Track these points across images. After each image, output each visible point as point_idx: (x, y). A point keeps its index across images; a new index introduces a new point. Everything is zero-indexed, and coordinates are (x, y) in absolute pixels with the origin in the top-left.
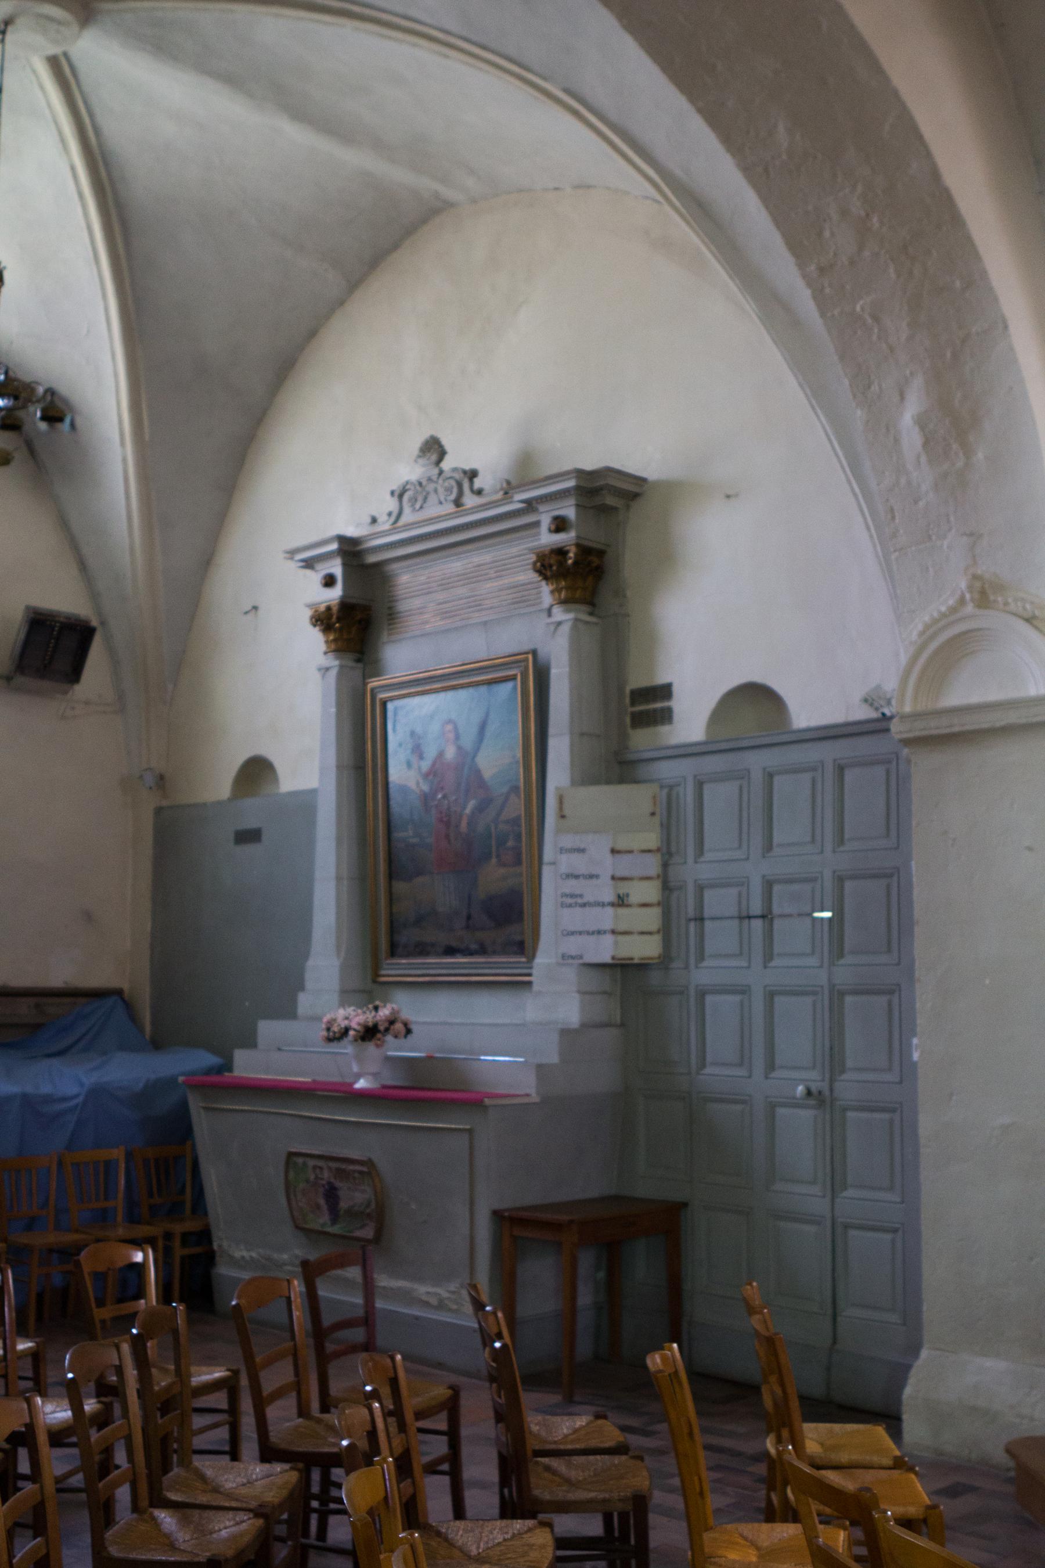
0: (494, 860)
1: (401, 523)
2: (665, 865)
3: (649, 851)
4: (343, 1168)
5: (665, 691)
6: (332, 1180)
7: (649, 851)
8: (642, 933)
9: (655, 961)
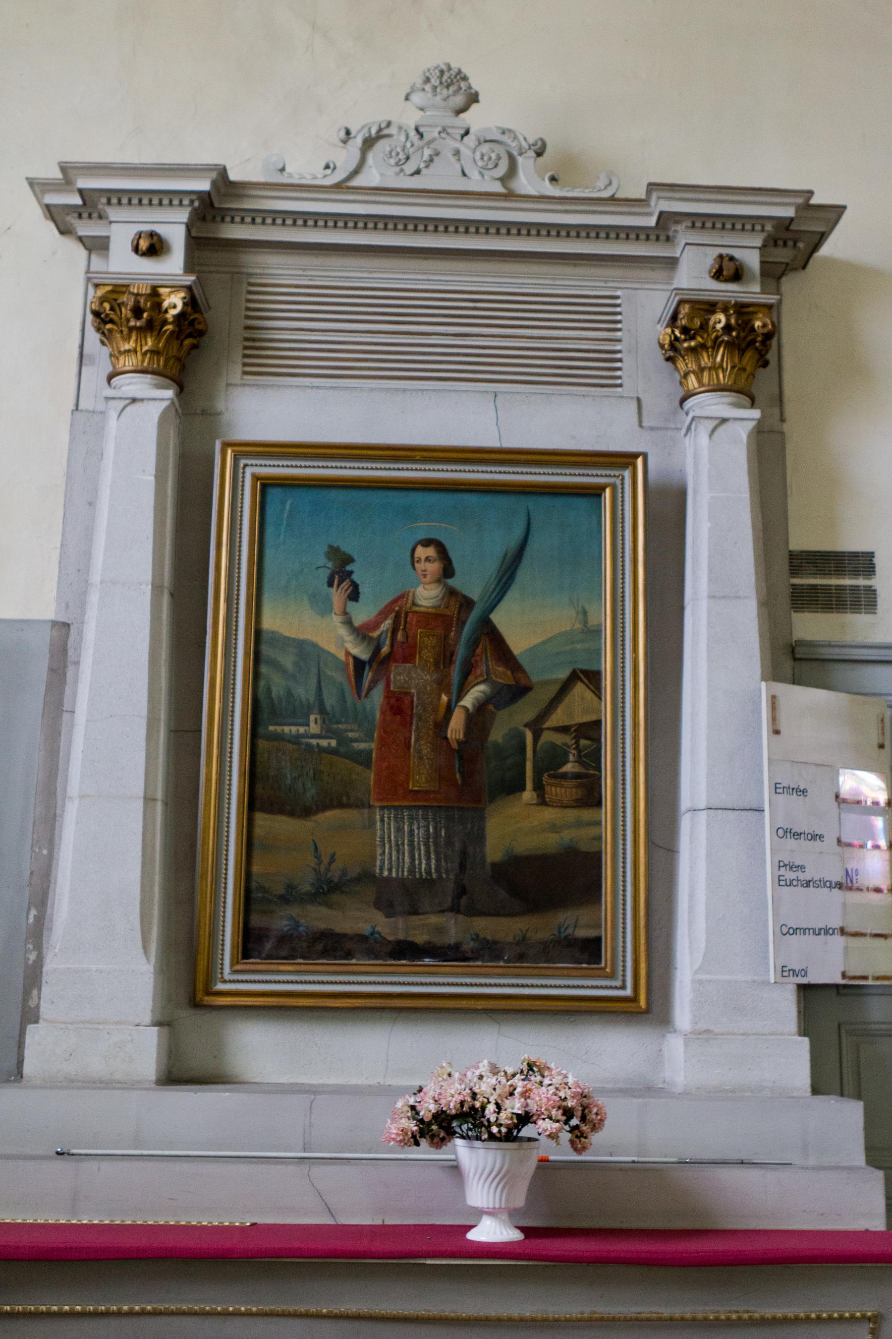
0: (528, 795)
1: (357, 182)
5: (864, 563)
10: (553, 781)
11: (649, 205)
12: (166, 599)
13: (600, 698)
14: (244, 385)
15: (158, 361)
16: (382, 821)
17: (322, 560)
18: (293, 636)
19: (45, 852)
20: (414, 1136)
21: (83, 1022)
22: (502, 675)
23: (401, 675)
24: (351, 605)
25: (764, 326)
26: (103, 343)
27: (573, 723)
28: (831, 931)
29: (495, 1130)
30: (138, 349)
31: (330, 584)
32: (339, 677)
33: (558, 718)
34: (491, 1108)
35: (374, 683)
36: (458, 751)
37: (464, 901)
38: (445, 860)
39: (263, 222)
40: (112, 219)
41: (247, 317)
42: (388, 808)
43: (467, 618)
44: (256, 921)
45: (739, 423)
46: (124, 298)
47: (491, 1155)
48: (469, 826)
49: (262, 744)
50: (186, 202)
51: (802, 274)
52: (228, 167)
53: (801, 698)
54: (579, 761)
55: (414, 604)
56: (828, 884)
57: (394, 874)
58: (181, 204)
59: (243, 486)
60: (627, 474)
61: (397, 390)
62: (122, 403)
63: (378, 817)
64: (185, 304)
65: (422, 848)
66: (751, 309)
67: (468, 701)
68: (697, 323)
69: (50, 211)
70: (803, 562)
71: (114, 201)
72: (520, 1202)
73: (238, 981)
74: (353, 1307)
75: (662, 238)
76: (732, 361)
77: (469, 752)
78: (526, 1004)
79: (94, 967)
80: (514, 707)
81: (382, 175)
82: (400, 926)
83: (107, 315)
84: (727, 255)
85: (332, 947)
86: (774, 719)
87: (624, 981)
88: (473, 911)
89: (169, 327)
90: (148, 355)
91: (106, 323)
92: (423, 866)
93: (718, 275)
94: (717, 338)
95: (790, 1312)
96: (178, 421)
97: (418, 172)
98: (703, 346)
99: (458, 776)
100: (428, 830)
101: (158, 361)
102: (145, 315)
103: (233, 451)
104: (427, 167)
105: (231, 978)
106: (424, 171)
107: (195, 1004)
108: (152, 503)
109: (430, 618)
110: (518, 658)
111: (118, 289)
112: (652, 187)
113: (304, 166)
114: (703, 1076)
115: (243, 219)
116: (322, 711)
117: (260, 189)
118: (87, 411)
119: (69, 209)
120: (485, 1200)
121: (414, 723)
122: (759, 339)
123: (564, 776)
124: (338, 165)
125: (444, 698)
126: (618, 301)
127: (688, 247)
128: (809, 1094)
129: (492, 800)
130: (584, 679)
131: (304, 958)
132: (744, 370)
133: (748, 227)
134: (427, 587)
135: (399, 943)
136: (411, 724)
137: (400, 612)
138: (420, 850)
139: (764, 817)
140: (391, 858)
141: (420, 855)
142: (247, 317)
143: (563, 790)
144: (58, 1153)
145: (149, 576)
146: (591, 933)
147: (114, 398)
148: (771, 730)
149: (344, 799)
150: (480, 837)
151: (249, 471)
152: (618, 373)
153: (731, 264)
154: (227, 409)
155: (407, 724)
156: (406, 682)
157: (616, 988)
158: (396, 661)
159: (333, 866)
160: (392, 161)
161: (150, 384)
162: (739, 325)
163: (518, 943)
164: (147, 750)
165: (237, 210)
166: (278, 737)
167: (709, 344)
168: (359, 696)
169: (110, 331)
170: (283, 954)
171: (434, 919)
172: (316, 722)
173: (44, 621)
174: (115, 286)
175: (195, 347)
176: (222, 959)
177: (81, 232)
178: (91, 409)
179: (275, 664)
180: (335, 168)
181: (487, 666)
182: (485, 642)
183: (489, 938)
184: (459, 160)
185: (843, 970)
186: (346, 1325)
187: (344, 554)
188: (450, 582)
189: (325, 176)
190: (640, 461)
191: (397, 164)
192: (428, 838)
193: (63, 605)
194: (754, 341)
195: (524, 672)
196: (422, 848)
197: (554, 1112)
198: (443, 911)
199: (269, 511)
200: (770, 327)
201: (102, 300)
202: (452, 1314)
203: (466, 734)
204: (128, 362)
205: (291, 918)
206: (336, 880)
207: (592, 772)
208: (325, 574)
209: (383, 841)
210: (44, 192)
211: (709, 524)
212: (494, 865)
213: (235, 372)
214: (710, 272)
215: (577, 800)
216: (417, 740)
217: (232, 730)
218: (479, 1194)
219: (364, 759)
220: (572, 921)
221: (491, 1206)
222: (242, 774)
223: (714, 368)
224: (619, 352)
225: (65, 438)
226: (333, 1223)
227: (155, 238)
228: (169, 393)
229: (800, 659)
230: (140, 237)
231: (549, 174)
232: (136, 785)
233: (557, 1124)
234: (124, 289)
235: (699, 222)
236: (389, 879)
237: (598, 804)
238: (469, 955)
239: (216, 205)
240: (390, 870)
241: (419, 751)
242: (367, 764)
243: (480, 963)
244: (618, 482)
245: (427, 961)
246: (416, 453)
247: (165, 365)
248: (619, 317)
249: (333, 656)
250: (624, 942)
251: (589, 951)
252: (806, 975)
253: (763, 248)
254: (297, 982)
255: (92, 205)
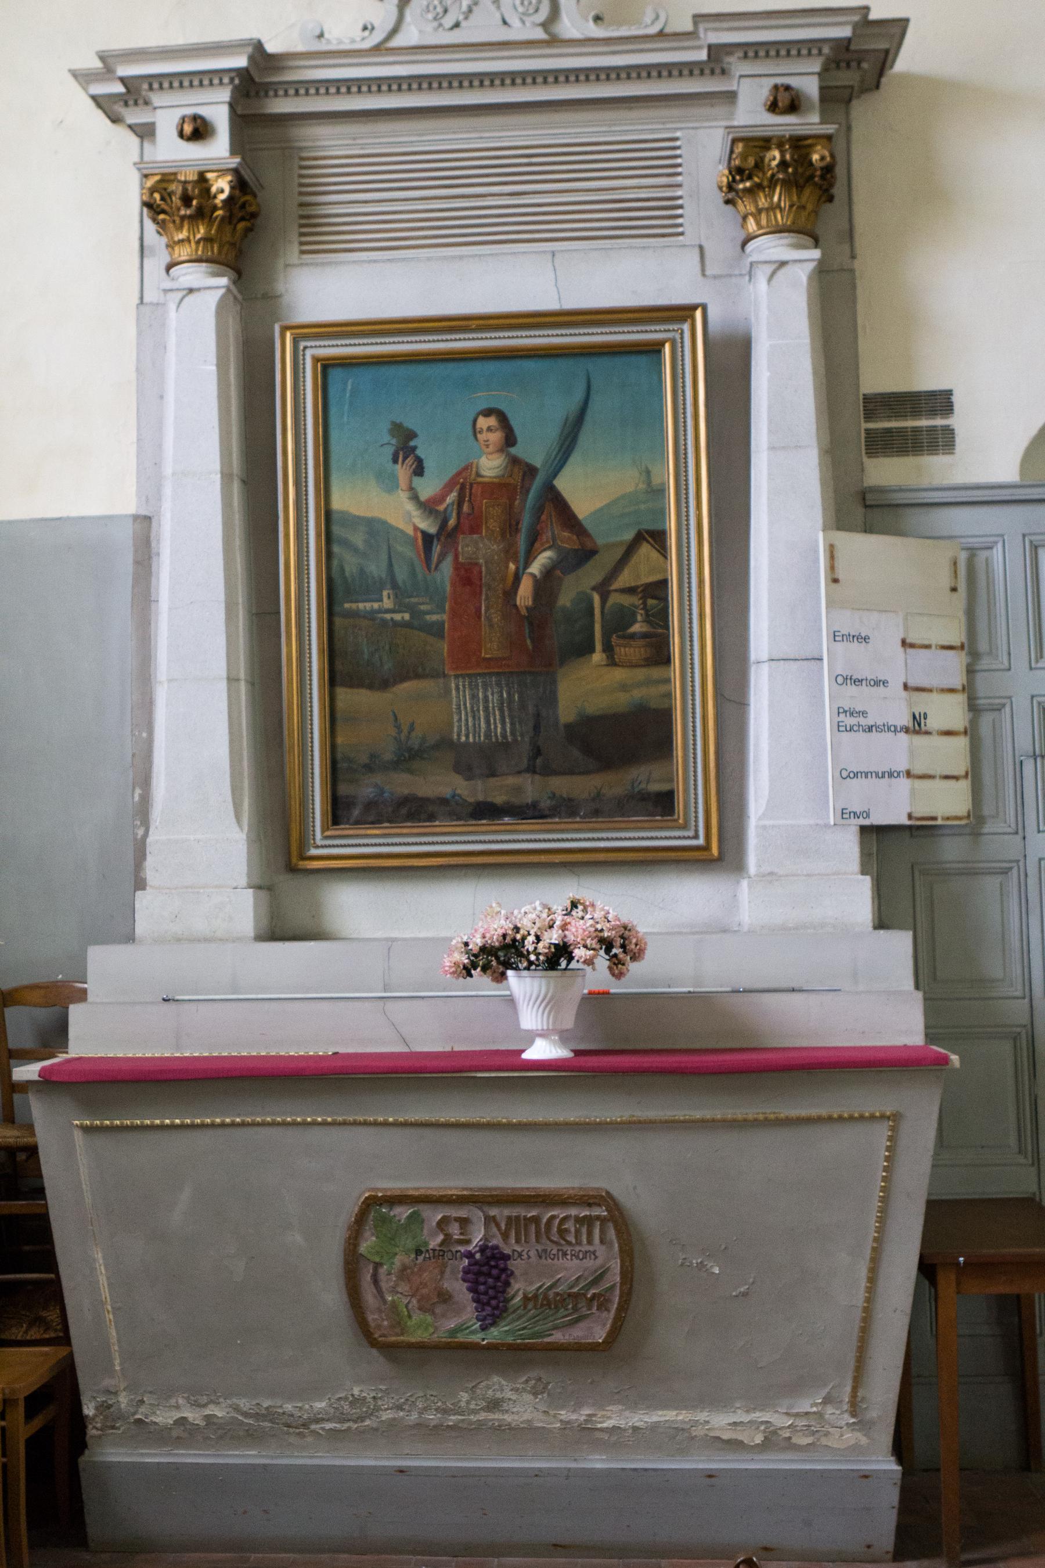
0: (598, 656)
2: (971, 671)
3: (951, 648)
4: (525, 1209)
5: (941, 402)
6: (497, 1241)
7: (951, 648)
8: (947, 777)
9: (963, 822)
10: (622, 641)
11: (698, 38)
12: (236, 486)
13: (666, 557)
14: (302, 264)
15: (212, 251)
16: (457, 689)
17: (387, 438)
18: (362, 514)
19: (144, 735)
20: (465, 968)
21: (187, 887)
22: (567, 539)
23: (467, 547)
24: (417, 481)
25: (822, 158)
26: (159, 232)
27: (639, 583)
28: (895, 774)
29: (533, 957)
30: (192, 237)
31: (395, 461)
32: (408, 552)
33: (625, 579)
34: (531, 939)
35: (442, 556)
36: (527, 618)
37: (539, 761)
38: (520, 723)
39: (307, 94)
40: (156, 105)
41: (301, 194)
42: (463, 676)
43: (531, 484)
44: (343, 789)
45: (799, 265)
46: (173, 187)
47: (536, 983)
48: (541, 690)
49: (338, 621)
50: (226, 80)
51: (876, 96)
52: (263, 41)
53: (858, 545)
54: (647, 620)
55: (478, 475)
56: (893, 729)
57: (471, 740)
58: (221, 83)
59: (304, 368)
60: (686, 327)
61: (454, 257)
62: (180, 295)
63: (453, 685)
64: (232, 188)
65: (497, 713)
66: (809, 142)
67: (535, 568)
68: (751, 161)
69: (97, 100)
70: (881, 404)
71: (156, 86)
72: (569, 1022)
73: (330, 846)
74: (413, 1117)
75: (718, 71)
76: (790, 200)
77: (538, 620)
78: (601, 857)
79: (192, 837)
80: (580, 572)
81: (420, 31)
82: (480, 788)
83: (159, 206)
84: (782, 85)
85: (415, 811)
86: (832, 567)
87: (697, 831)
88: (548, 771)
89: (219, 213)
90: (202, 244)
91: (159, 213)
92: (499, 730)
93: (773, 107)
94: (773, 175)
95: (814, 1112)
96: (239, 308)
97: (457, 25)
98: (759, 186)
99: (528, 642)
100: (502, 696)
101: (212, 248)
102: (194, 202)
103: (292, 334)
104: (466, 18)
105: (325, 844)
106: (464, 24)
107: (292, 869)
108: (215, 393)
109: (494, 489)
110: (584, 523)
111: (167, 178)
112: (698, 18)
113: (343, 32)
114: (773, 915)
115: (286, 91)
116: (395, 586)
117: (303, 59)
118: (151, 304)
119: (111, 97)
120: (535, 1021)
121: (484, 592)
122: (818, 173)
123: (632, 636)
124: (376, 25)
125: (512, 566)
126: (678, 143)
127: (743, 80)
128: (871, 929)
129: (562, 663)
130: (650, 539)
131: (390, 822)
132: (804, 207)
133: (804, 52)
134: (490, 457)
135: (479, 804)
136: (481, 593)
137: (464, 483)
138: (494, 714)
139: (822, 668)
140: (467, 724)
141: (495, 720)
142: (301, 194)
143: (632, 650)
144: (164, 1000)
145: (217, 466)
146: (664, 787)
147: (171, 290)
148: (829, 578)
149: (420, 670)
150: (551, 699)
151: (309, 353)
152: (680, 221)
153: (787, 94)
154: (287, 291)
155: (476, 594)
156: (475, 553)
157: (689, 838)
158: (463, 533)
159: (413, 734)
160: (430, 16)
161: (207, 273)
162: (795, 161)
163: (593, 800)
164: (227, 632)
165: (280, 83)
166: (355, 614)
167: (765, 183)
168: (429, 570)
169: (164, 221)
170: (370, 819)
171: (511, 780)
172: (389, 598)
173: (126, 516)
174: (163, 175)
175: (249, 230)
176: (314, 826)
177: (131, 120)
178: (155, 301)
179: (346, 543)
180: (373, 28)
181: (553, 533)
182: (549, 508)
183: (565, 796)
184: (499, 8)
185: (909, 811)
186: (408, 1131)
187: (407, 429)
188: (513, 450)
189: (363, 39)
190: (698, 314)
191: (435, 19)
192: (502, 704)
193: (144, 498)
194: (812, 177)
195: (589, 535)
196: (497, 713)
197: (589, 942)
198: (519, 772)
199: (332, 391)
200: (828, 159)
201: (152, 191)
202: (504, 1120)
203: (534, 600)
204: (184, 252)
205: (376, 786)
206: (416, 747)
207: (660, 631)
208: (389, 451)
209: (459, 708)
210: (88, 82)
211: (769, 374)
212: (568, 726)
213: (292, 253)
214: (765, 105)
215: (646, 659)
216: (487, 609)
217: (309, 609)
218: (530, 1019)
219: (436, 631)
220: (646, 777)
221: (540, 1028)
222: (321, 651)
223: (772, 208)
224: (680, 197)
225: (132, 331)
226: (407, 1050)
227: (199, 121)
228: (224, 281)
229: (871, 506)
230: (184, 122)
231: (593, 14)
232: (219, 666)
233: (592, 952)
234: (172, 177)
235: (752, 51)
236: (467, 744)
237: (667, 661)
238: (547, 812)
239: (257, 80)
240: (467, 736)
241: (489, 619)
242: (440, 635)
243: (557, 820)
244: (678, 336)
245: (506, 819)
246: (470, 323)
247: (220, 252)
248: (679, 161)
249: (402, 532)
250: (696, 794)
251: (663, 804)
252: (868, 816)
253: (825, 70)
254: (384, 845)
255: (135, 91)
